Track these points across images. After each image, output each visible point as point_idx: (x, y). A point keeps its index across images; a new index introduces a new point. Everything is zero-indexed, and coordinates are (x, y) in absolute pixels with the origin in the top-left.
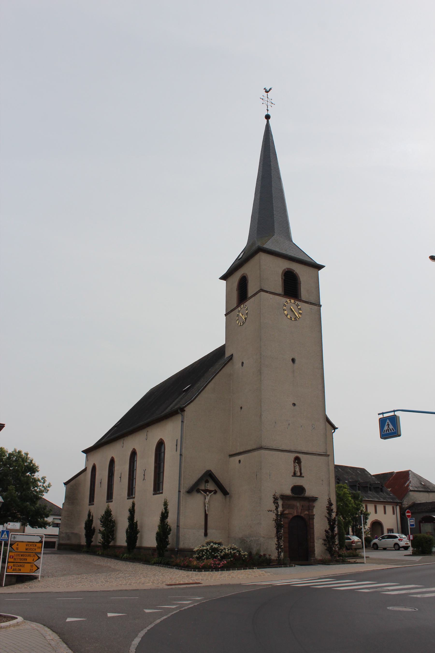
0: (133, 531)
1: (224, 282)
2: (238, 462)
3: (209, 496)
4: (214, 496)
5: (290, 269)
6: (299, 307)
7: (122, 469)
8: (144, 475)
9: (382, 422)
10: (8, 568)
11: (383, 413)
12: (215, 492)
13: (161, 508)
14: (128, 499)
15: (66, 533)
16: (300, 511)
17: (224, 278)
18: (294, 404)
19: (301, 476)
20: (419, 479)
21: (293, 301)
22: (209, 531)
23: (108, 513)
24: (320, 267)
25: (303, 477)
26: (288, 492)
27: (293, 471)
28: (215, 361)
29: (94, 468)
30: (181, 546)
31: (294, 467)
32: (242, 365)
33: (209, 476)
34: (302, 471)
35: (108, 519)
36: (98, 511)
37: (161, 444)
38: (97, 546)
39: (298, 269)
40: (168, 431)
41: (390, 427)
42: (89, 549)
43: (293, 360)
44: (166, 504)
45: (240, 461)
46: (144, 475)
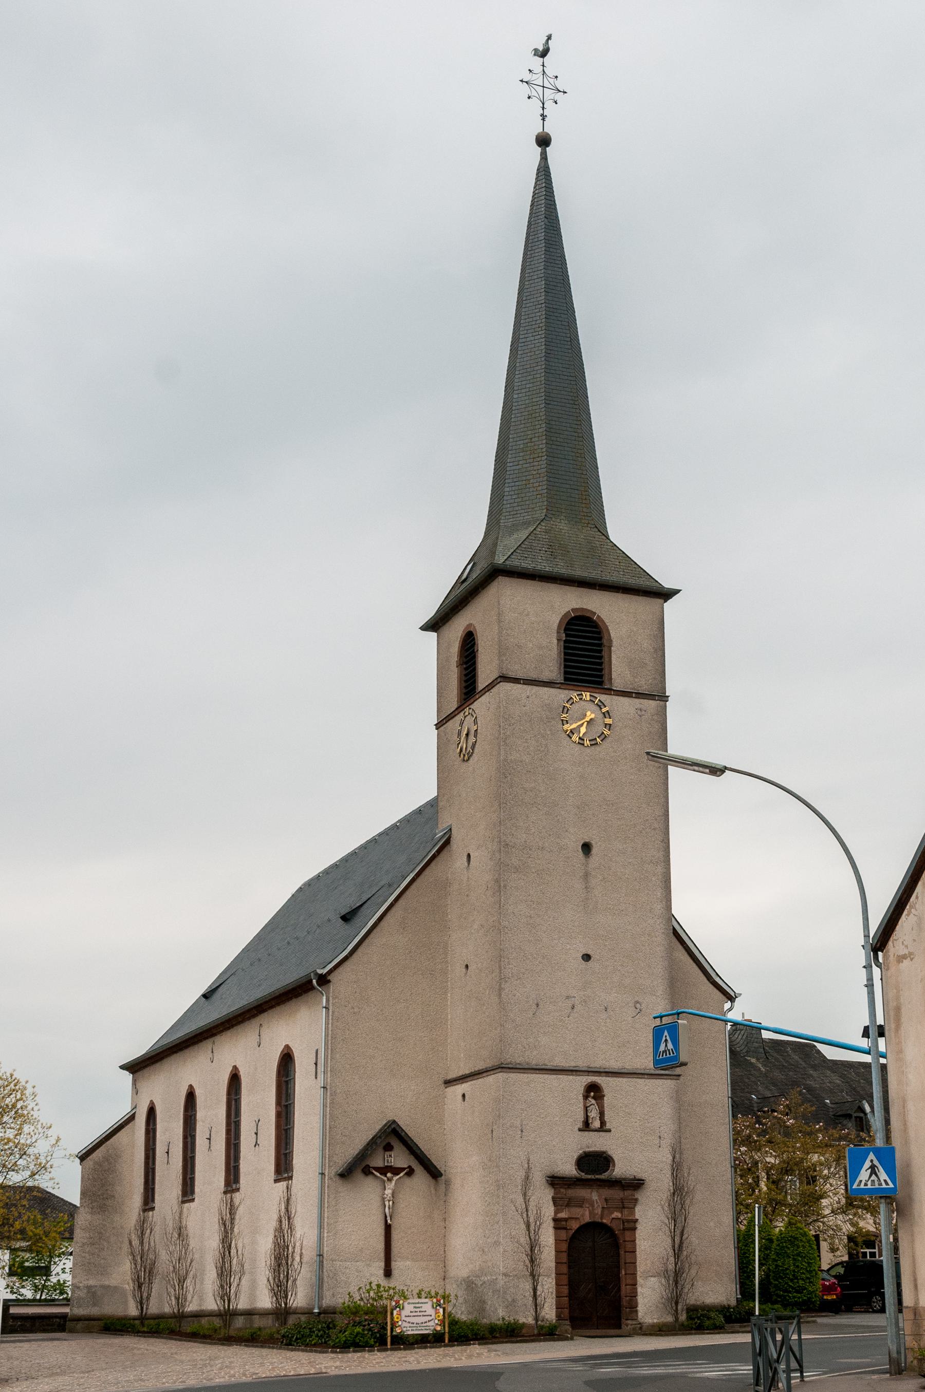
1: (434, 635)
2: (460, 1097)
3: (394, 1182)
4: (407, 1181)
5: (582, 609)
6: (604, 710)
7: (212, 1116)
8: (256, 1134)
12: (410, 1172)
14: (276, 1181)
15: (89, 1288)
16: (599, 1211)
19: (603, 1128)
21: (587, 696)
22: (394, 1265)
24: (667, 595)
25: (609, 1131)
26: (569, 1169)
27: (581, 1117)
31: (586, 1109)
33: (392, 1135)
34: (606, 1118)
39: (600, 605)
40: (300, 1030)
43: (587, 848)
46: (256, 1134)
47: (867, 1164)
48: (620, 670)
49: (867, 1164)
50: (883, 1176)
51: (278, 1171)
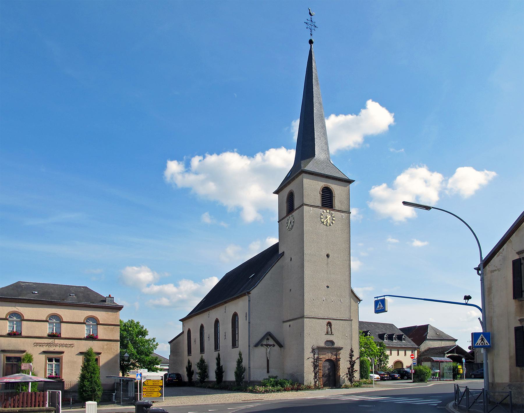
0: (220, 372)
1: (277, 195)
7: (209, 332)
9: (376, 303)
10: (143, 394)
11: (377, 297)
12: (274, 346)
13: (238, 357)
17: (276, 192)
18: (328, 287)
20: (435, 330)
21: (328, 211)
23: (202, 361)
24: (349, 182)
26: (322, 345)
27: (326, 331)
28: (272, 255)
29: (189, 331)
30: (252, 379)
32: (291, 260)
35: (202, 364)
36: (195, 358)
37: (235, 315)
38: (196, 382)
40: (239, 306)
41: (380, 306)
42: (191, 384)
43: (328, 256)
44: (240, 354)
45: (290, 326)
47: (480, 338)
48: (337, 204)
49: (480, 338)
50: (486, 341)
51: (201, 352)
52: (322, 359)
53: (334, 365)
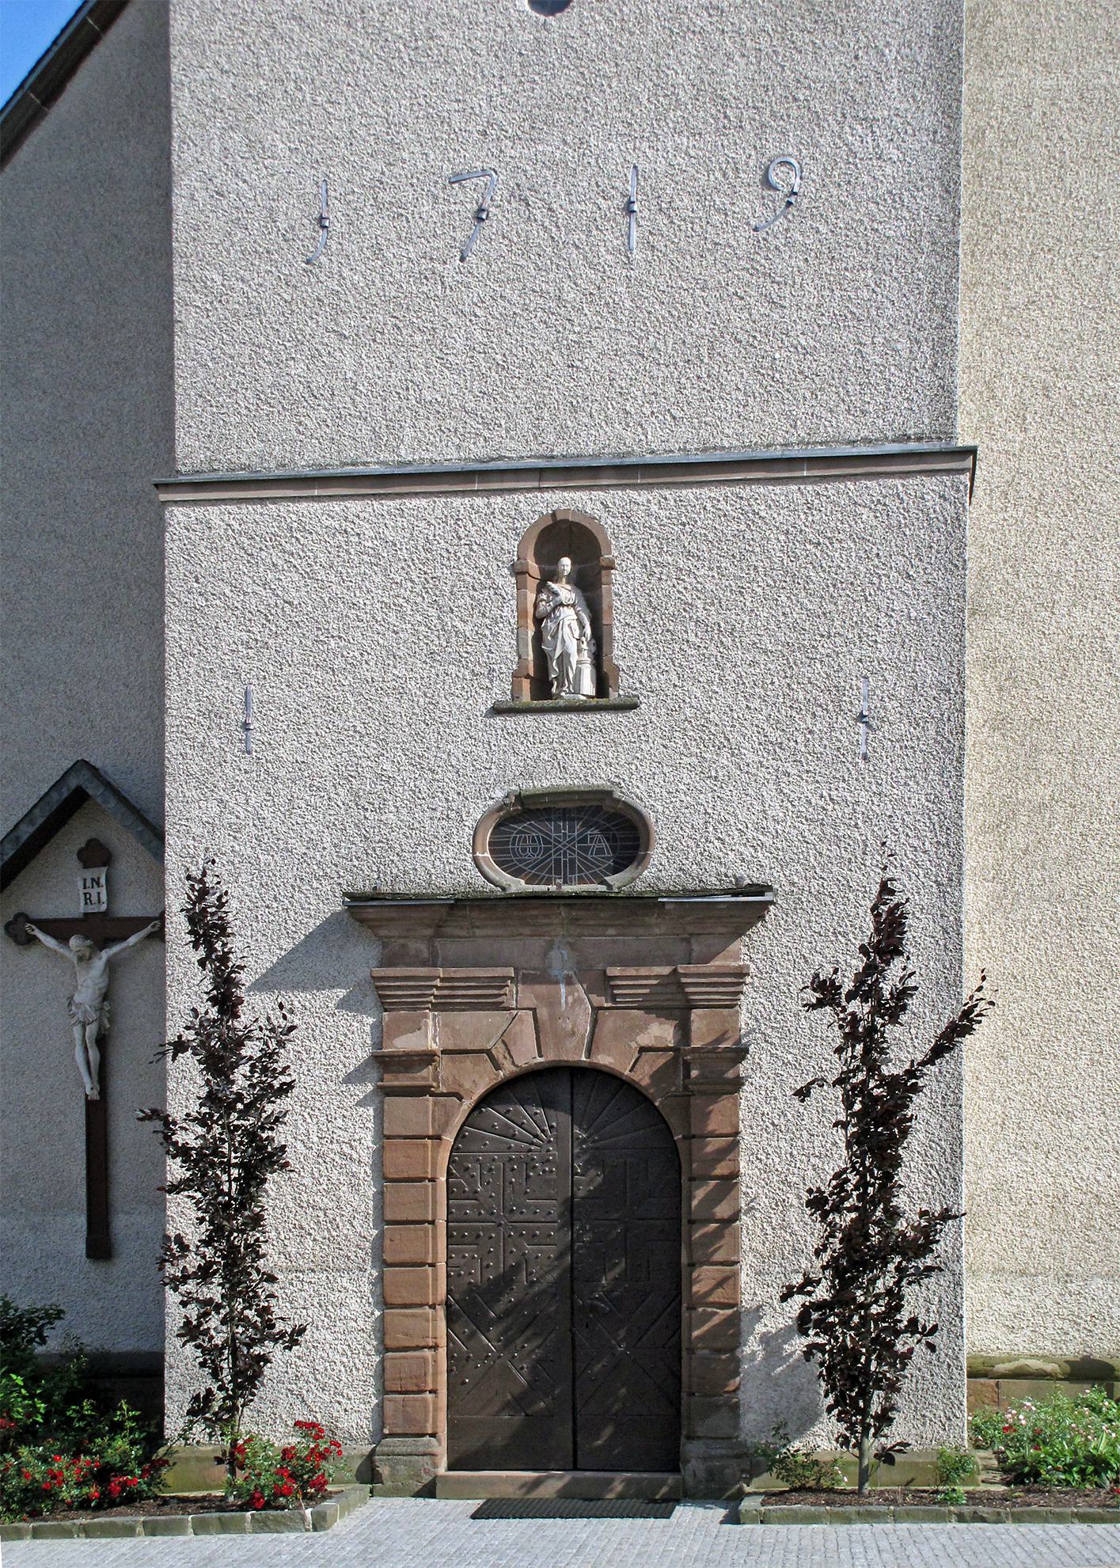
26: (449, 858)
27: (507, 652)
34: (618, 654)
35: (803, 1323)
52: (445, 1072)
53: (648, 1150)
